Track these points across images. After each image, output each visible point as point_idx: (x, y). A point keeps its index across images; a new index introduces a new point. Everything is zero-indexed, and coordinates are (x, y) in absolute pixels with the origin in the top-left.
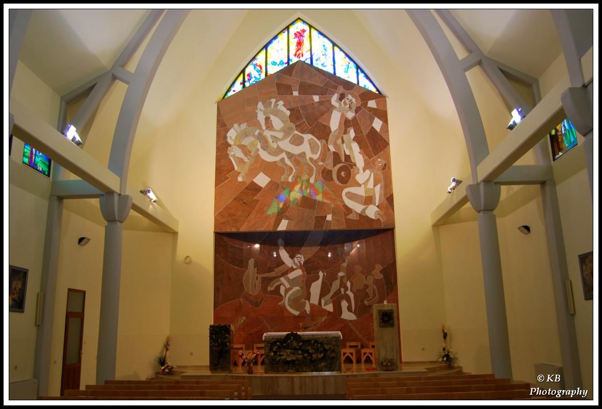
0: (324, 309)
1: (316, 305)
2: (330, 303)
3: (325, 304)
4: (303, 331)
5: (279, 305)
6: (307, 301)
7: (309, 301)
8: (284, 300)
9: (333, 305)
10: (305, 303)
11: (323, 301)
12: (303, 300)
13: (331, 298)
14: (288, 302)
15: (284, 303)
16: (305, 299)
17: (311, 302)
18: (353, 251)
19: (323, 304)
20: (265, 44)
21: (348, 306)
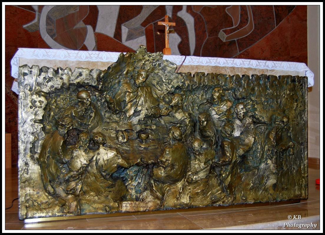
0: (124, 46)
1: (111, 39)
2: (140, 35)
3: (130, 37)
4: (225, 28)
5: (25, 31)
6: (89, 28)
7: (94, 28)
8: (36, 20)
9: (147, 37)
10: (85, 31)
11: (125, 31)
12: (81, 25)
13: (144, 24)
14: (48, 24)
15: (37, 25)
16: (86, 22)
17: (98, 30)
18: (53, 167)
19: (124, 36)
20: (93, 48)
21: (181, 43)
